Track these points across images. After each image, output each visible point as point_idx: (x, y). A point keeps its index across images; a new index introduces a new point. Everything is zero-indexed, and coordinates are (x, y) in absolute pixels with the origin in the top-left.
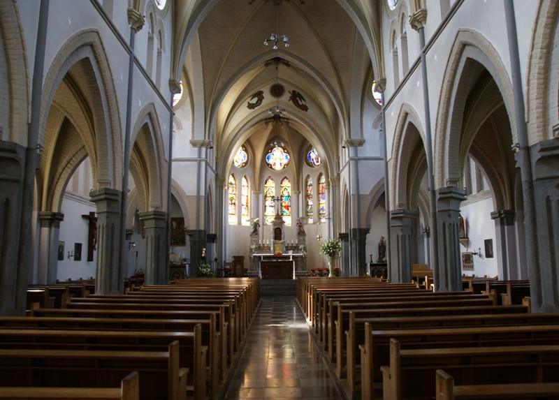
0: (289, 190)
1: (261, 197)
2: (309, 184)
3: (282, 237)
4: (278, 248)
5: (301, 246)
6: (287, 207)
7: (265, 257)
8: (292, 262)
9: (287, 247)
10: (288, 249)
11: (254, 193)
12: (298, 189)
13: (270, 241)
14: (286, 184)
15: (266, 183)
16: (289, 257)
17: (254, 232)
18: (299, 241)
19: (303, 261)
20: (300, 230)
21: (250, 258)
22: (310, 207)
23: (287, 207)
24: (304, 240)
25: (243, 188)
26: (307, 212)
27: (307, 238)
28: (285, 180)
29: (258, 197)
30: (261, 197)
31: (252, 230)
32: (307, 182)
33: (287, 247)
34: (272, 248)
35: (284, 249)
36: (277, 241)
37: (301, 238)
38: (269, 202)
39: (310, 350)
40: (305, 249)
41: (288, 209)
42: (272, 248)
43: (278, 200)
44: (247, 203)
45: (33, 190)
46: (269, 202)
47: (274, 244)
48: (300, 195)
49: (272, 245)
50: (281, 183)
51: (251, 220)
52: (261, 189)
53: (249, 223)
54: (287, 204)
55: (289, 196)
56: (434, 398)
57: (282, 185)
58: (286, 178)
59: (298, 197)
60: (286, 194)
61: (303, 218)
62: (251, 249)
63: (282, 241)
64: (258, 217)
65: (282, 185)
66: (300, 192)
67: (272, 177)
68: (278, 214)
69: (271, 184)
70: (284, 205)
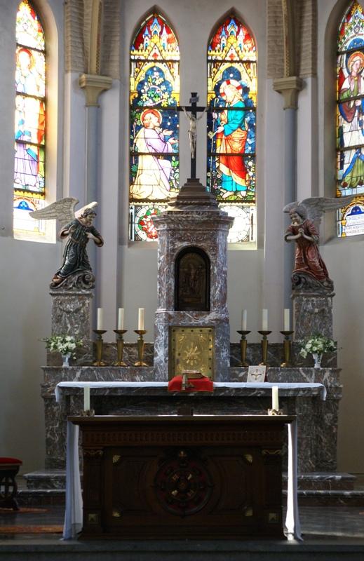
0: (250, 79)
1: (112, 105)
2: (347, 42)
3: (215, 293)
4: (192, 352)
5: (311, 346)
6: (240, 162)
7: (99, 398)
8: (278, 425)
9: (236, 349)
10: (241, 356)
11: (78, 84)
12: (295, 70)
13: (148, 318)
14: (236, 45)
15: (138, 41)
16: (263, 399)
17: (70, 270)
18: (299, 317)
19: (319, 420)
20: (304, 261)
21: (49, 400)
22: (349, 156)
23: (240, 162)
24: (325, 315)
25: (22, 57)
26: (336, 183)
27: (337, 305)
28: (231, 28)
29: (95, 108)
30: (112, 105)
31: (61, 262)
32: (336, 35)
33: (236, 349)
34: (161, 354)
35: (225, 354)
36: (190, 317)
37: (311, 304)
38: (150, 137)
39: (184, 383)
40: (329, 357)
41: (243, 172)
42: (161, 354)
43: (194, 109)
44: (43, 134)
45: (287, 447)
46: (150, 137)
47: (171, 330)
48: (305, 101)
49: (162, 337)
50: (212, 45)
51: (59, 209)
52: (115, 68)
53: (52, 224)
54: (237, 147)
55: (247, 107)
56: (283, 491)
57: (216, 55)
58: (232, 17)
59: (294, 107)
60: (231, 94)
61: (315, 203)
62: (55, 358)
63: (212, 316)
64: (96, 193)
65: (216, 55)
66: (301, 85)
67: (169, 11)
68: (193, 179)
69: (159, 44)
70: (221, 149)
